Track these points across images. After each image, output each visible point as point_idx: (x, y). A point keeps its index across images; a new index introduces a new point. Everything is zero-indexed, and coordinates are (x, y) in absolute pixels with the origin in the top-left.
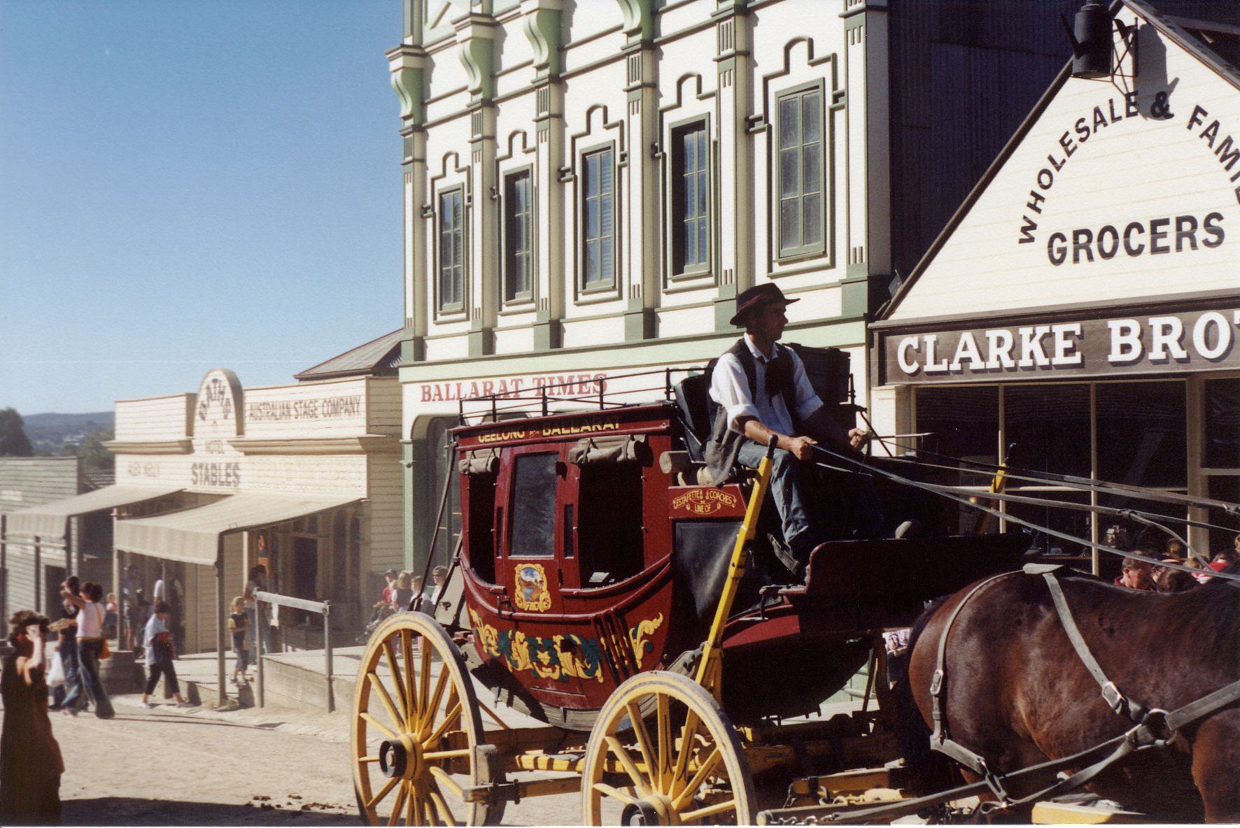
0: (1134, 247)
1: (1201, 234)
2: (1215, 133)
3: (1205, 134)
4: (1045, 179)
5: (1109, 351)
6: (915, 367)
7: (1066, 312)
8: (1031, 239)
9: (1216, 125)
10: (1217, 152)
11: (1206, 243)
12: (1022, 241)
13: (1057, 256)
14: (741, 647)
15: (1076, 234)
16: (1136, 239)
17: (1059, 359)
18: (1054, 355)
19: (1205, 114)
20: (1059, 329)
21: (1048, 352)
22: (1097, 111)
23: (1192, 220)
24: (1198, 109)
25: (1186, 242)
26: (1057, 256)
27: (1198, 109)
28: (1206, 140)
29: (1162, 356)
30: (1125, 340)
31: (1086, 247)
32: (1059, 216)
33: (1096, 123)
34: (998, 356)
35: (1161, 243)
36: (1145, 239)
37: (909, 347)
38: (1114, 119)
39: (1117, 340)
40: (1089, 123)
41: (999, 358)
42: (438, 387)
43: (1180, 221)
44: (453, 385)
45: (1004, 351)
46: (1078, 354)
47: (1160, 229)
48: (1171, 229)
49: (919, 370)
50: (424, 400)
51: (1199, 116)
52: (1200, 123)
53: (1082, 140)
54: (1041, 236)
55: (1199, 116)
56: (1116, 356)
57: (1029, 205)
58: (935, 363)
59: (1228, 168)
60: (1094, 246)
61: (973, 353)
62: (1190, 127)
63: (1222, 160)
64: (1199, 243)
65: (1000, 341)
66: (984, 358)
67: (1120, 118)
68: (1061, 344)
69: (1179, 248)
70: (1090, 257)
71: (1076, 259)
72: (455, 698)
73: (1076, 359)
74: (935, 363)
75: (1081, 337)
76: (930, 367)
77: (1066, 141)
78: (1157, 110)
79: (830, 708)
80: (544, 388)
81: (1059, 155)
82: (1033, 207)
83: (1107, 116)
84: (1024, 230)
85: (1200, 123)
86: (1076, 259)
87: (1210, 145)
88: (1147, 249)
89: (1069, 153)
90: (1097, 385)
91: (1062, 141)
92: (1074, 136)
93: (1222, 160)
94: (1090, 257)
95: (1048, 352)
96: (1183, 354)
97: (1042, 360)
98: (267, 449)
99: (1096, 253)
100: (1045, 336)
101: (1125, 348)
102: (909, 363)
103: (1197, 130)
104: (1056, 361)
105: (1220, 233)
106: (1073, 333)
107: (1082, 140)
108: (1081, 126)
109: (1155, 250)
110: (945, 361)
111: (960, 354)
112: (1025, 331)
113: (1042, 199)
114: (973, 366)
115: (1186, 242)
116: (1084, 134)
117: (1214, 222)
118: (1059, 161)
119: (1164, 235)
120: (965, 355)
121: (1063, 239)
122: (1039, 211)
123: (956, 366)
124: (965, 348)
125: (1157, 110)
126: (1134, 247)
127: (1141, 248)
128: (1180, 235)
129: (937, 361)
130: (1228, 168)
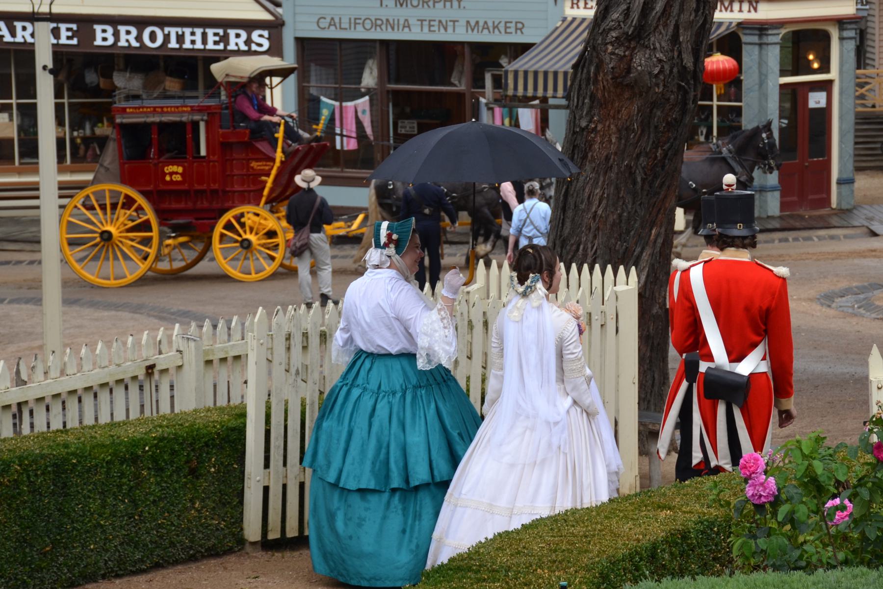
5: (94, 39)
17: (210, 46)
18: (184, 43)
21: (204, 41)
29: (236, 48)
30: (104, 35)
39: (99, 35)
43: (516, 23)
47: (508, 25)
56: (98, 42)
65: (24, 28)
68: (211, 38)
72: (93, 223)
73: (75, 41)
79: (301, 132)
95: (204, 41)
96: (137, 45)
98: (869, 158)
101: (105, 39)
128: (516, 29)
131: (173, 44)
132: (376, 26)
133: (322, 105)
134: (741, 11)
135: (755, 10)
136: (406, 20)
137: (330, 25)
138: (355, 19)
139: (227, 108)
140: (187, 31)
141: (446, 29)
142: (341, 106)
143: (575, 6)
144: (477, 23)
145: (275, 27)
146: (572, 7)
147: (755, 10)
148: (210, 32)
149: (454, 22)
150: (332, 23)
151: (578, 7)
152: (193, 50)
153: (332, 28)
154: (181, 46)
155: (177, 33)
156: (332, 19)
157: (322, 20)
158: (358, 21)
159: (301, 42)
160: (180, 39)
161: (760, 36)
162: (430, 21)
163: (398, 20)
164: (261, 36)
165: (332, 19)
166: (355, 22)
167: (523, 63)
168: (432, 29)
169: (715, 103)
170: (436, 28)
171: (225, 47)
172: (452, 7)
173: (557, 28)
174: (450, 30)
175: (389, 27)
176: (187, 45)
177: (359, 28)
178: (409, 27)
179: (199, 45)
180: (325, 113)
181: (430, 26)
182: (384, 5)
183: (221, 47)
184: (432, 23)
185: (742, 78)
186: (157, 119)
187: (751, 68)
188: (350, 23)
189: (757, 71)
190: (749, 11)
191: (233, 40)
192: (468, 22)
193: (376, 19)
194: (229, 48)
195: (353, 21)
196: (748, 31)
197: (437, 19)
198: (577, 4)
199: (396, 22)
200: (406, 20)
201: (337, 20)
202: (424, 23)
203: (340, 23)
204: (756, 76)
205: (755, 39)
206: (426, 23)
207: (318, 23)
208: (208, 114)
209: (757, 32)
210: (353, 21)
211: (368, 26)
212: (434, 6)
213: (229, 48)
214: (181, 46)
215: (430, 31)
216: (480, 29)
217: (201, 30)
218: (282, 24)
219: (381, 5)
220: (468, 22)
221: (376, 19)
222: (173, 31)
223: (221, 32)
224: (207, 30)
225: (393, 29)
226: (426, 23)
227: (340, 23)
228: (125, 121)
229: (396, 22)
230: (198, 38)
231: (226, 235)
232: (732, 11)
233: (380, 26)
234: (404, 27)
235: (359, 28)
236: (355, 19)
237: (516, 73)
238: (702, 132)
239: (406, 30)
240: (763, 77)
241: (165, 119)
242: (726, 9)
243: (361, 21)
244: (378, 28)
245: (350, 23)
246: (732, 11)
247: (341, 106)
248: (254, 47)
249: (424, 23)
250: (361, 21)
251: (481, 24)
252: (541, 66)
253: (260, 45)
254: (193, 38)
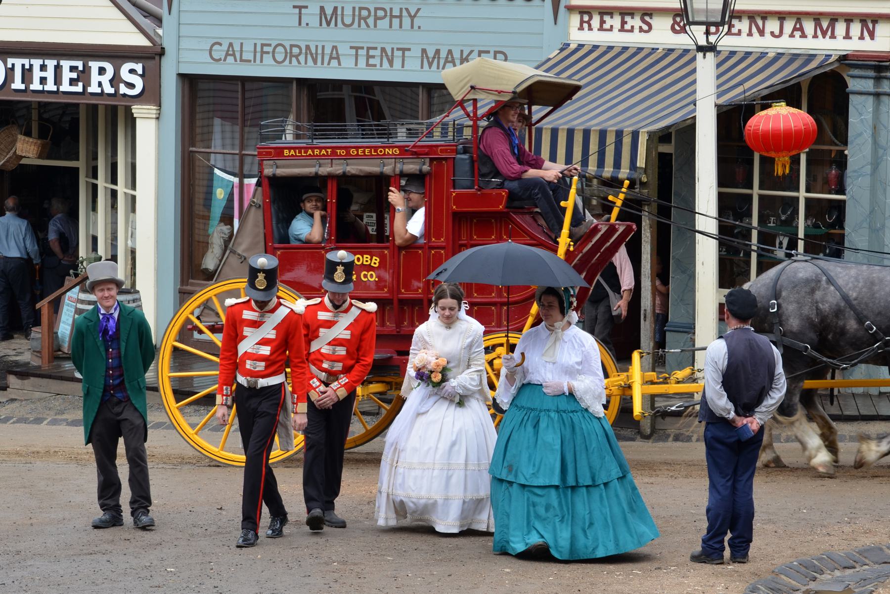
7: (868, 56)
17: (65, 87)
21: (58, 81)
29: (99, 90)
42: (223, 146)
44: (367, 151)
46: (80, 84)
68: (67, 75)
78: (677, 28)
80: (817, 302)
93: (328, 24)
95: (58, 81)
106: (77, 68)
125: (677, 28)
131: (18, 85)
132: (292, 56)
133: (215, 183)
134: (847, 36)
135: (872, 36)
136: (335, 48)
137: (227, 55)
138: (263, 45)
139: (465, 151)
140: (37, 63)
141: (391, 63)
142: (241, 184)
143: (586, 26)
144: (438, 52)
145: (151, 57)
146: (581, 28)
147: (872, 36)
148: (66, 64)
149: (404, 50)
150: (230, 52)
151: (590, 29)
152: (43, 92)
153: (230, 59)
154: (58, 89)
155: (23, 65)
156: (231, 45)
157: (216, 47)
158: (266, 49)
159: (191, 83)
160: (27, 74)
161: (878, 79)
162: (369, 49)
163: (323, 47)
164: (132, 71)
165: (231, 45)
166: (261, 50)
167: (564, 118)
168: (371, 61)
169: (802, 194)
170: (376, 61)
171: (84, 88)
172: (401, 26)
173: (549, 59)
174: (397, 63)
175: (385, 60)
176: (36, 86)
177: (268, 59)
178: (338, 58)
179: (50, 86)
180: (220, 194)
181: (369, 57)
182: (303, 24)
183: (79, 88)
184: (372, 53)
185: (846, 152)
186: (338, 168)
187: (860, 134)
188: (255, 52)
189: (870, 140)
190: (862, 38)
191: (95, 77)
192: (424, 51)
193: (292, 46)
194: (90, 90)
195: (259, 49)
196: (856, 72)
197: (379, 47)
198: (589, 23)
199: (320, 51)
200: (335, 48)
201: (237, 48)
202: (360, 52)
203: (241, 51)
204: (868, 149)
205: (868, 85)
206: (362, 52)
207: (211, 51)
208: (432, 160)
209: (872, 73)
210: (259, 49)
211: (280, 58)
212: (375, 26)
213: (90, 90)
214: (58, 89)
215: (368, 65)
216: (442, 62)
217: (55, 62)
218: (162, 53)
219: (300, 24)
220: (424, 51)
221: (292, 46)
222: (18, 63)
223: (79, 64)
224: (62, 63)
225: (315, 61)
226: (362, 52)
227: (241, 51)
228: (280, 172)
229: (320, 51)
230: (50, 74)
231: (837, 193)
232: (833, 36)
233: (297, 57)
234: (331, 58)
235: (268, 59)
236: (263, 45)
237: (554, 132)
238: (781, 243)
239: (334, 63)
240: (881, 152)
241: (353, 168)
242: (824, 34)
243: (270, 49)
244: (294, 59)
245: (255, 52)
246: (833, 36)
247: (241, 184)
248: (123, 89)
249: (360, 52)
250: (270, 49)
251: (443, 54)
252: (565, 123)
253: (131, 86)
254: (43, 74)
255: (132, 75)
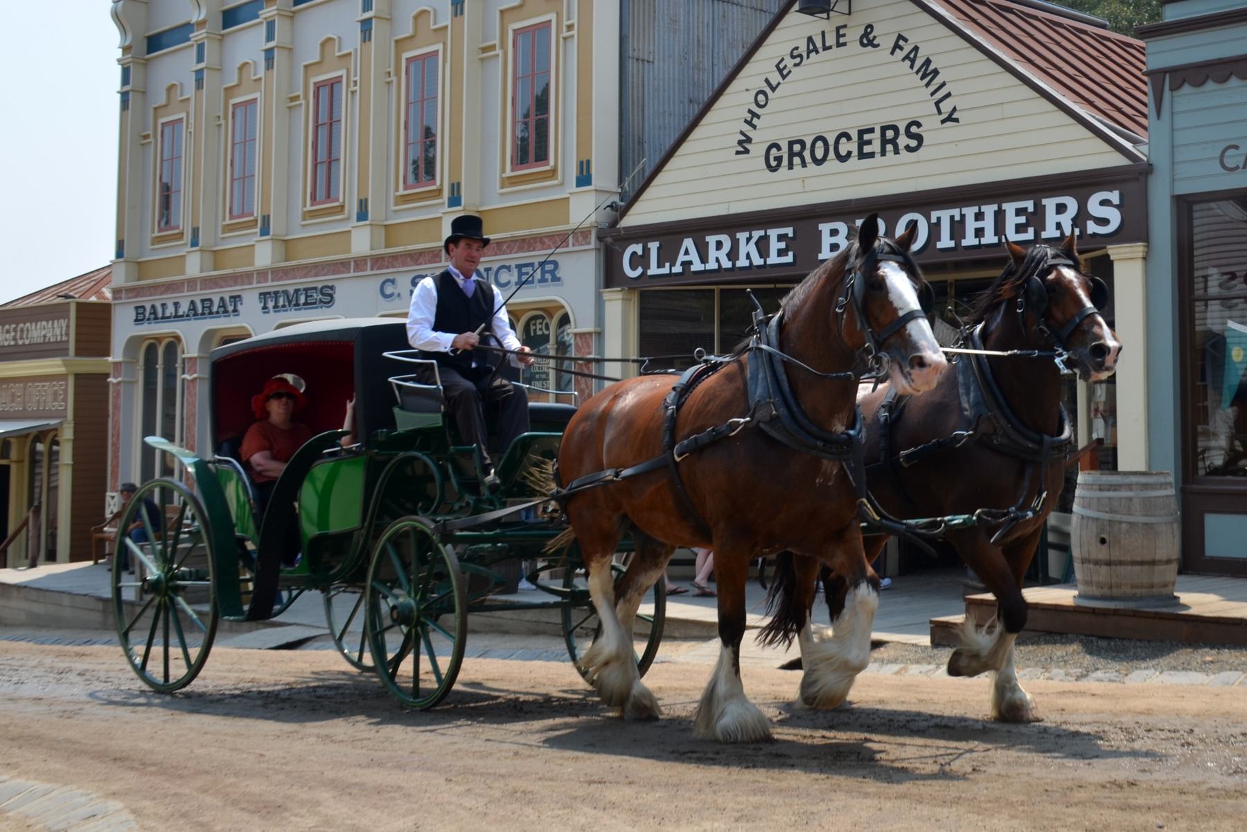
0: (843, 152)
1: (903, 141)
2: (915, 56)
3: (907, 57)
4: (761, 98)
6: (640, 270)
8: (747, 151)
9: (916, 49)
10: (917, 72)
11: (908, 148)
12: (738, 153)
13: (773, 163)
14: (534, 719)
15: (791, 144)
16: (844, 148)
17: (773, 259)
19: (906, 40)
20: (773, 233)
21: (764, 253)
22: (810, 39)
23: (895, 128)
24: (900, 37)
25: (889, 147)
26: (773, 163)
27: (900, 37)
28: (908, 63)
30: (834, 240)
31: (800, 155)
32: (777, 126)
33: (809, 52)
34: (718, 258)
35: (867, 149)
36: (853, 146)
37: (634, 253)
38: (825, 48)
39: (827, 240)
40: (803, 49)
41: (717, 260)
43: (884, 129)
45: (722, 255)
46: (791, 254)
47: (866, 137)
48: (876, 136)
49: (643, 274)
50: (136, 320)
51: (901, 43)
52: (901, 49)
53: (796, 65)
54: (757, 150)
55: (901, 43)
57: (758, 117)
58: (659, 267)
59: (928, 85)
60: (807, 154)
61: (694, 256)
62: (892, 53)
63: (922, 78)
64: (901, 146)
65: (719, 245)
66: (704, 260)
67: (830, 48)
68: (775, 245)
69: (883, 153)
70: (804, 164)
71: (791, 166)
73: (789, 259)
74: (659, 267)
75: (793, 239)
76: (654, 270)
77: (781, 66)
78: (865, 41)
81: (775, 78)
82: (749, 123)
83: (819, 45)
84: (740, 143)
85: (901, 49)
86: (791, 166)
87: (912, 67)
88: (855, 153)
89: (784, 77)
90: (722, 291)
91: (777, 66)
92: (789, 62)
93: (922, 78)
94: (804, 164)
95: (764, 253)
97: (758, 261)
99: (808, 158)
100: (761, 238)
102: (633, 268)
103: (900, 54)
104: (769, 261)
105: (919, 138)
107: (796, 65)
108: (795, 53)
109: (862, 155)
110: (667, 265)
111: (682, 258)
112: (742, 236)
113: (758, 117)
114: (693, 268)
115: (889, 147)
116: (798, 60)
117: (914, 129)
118: (774, 83)
119: (869, 142)
120: (687, 258)
121: (779, 148)
122: (754, 127)
123: (678, 269)
124: (687, 253)
125: (865, 41)
126: (843, 152)
127: (849, 154)
128: (884, 142)
129: (660, 265)
130: (928, 85)
222: (944, 216)
255: (1105, 210)
